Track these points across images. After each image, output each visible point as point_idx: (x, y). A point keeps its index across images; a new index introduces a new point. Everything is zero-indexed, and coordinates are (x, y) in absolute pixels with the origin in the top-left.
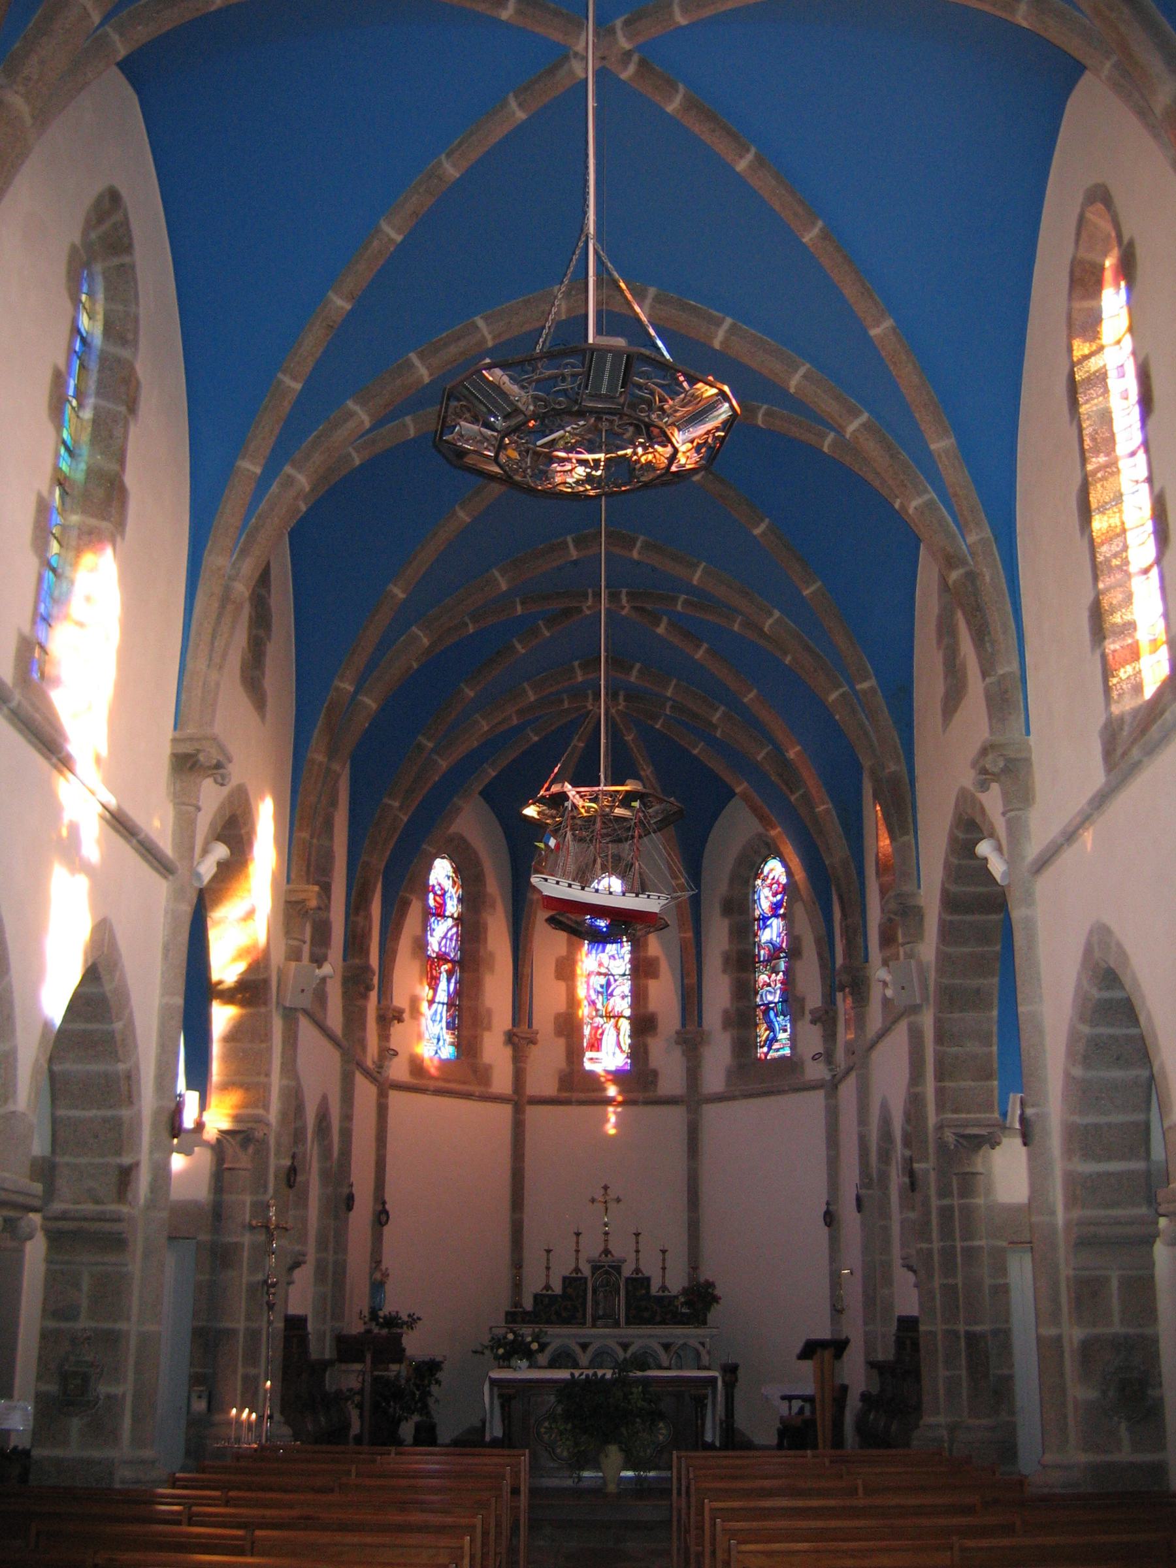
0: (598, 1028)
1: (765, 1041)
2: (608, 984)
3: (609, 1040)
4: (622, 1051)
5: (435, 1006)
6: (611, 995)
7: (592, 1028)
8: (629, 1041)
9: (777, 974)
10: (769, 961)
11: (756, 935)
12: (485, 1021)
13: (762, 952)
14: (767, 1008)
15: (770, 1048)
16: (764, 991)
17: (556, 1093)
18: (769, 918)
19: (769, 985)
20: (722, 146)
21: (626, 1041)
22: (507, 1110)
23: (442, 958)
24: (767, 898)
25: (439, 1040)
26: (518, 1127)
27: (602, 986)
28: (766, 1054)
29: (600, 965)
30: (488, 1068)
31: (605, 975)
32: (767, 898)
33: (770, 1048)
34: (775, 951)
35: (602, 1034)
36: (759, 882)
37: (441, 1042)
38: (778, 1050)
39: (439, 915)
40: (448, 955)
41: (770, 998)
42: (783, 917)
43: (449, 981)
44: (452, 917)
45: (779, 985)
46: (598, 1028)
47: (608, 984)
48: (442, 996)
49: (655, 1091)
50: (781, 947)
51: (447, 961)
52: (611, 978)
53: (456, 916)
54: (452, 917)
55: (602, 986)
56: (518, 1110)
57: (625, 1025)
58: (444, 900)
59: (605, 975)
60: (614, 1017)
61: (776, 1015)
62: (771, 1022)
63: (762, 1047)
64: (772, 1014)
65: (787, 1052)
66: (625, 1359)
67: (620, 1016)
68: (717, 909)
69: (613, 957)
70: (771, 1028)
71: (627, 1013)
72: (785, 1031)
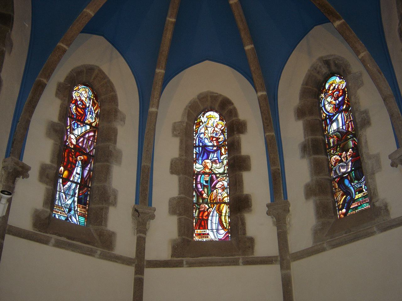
0: (204, 211)
1: (343, 205)
2: (212, 180)
3: (213, 220)
4: (224, 228)
5: (69, 183)
6: (214, 187)
7: (199, 212)
8: (228, 220)
9: (347, 151)
10: (338, 144)
11: (325, 130)
12: (112, 198)
13: (331, 140)
14: (342, 178)
15: (348, 209)
16: (337, 167)
17: (170, 258)
18: (334, 116)
19: (341, 161)
20: (245, 35)
21: (226, 220)
22: (130, 270)
23: (79, 150)
24: (330, 103)
25: (70, 210)
26: (139, 284)
27: (206, 182)
28: (345, 214)
29: (205, 167)
30: (112, 235)
31: (209, 174)
32: (330, 103)
33: (348, 209)
34: (342, 136)
35: (208, 215)
36: (323, 95)
37: (72, 212)
38: (356, 208)
39: (79, 121)
40: (85, 149)
41: (343, 170)
42: (346, 110)
43: (83, 168)
44: (90, 125)
45: (350, 159)
46: (204, 211)
47: (212, 180)
48: (77, 178)
49: (253, 253)
50: (348, 131)
51: (83, 154)
52: (214, 176)
53: (94, 125)
54: (90, 125)
55: (206, 182)
56: (139, 271)
57: (225, 209)
58: (85, 112)
59: (209, 174)
60: (216, 203)
61: (351, 181)
62: (347, 188)
63: (341, 210)
64: (347, 182)
65: (366, 206)
66: (94, 129)
67: (222, 202)
68: (292, 115)
69: (214, 162)
70: (347, 192)
71: (227, 200)
72: (361, 191)
